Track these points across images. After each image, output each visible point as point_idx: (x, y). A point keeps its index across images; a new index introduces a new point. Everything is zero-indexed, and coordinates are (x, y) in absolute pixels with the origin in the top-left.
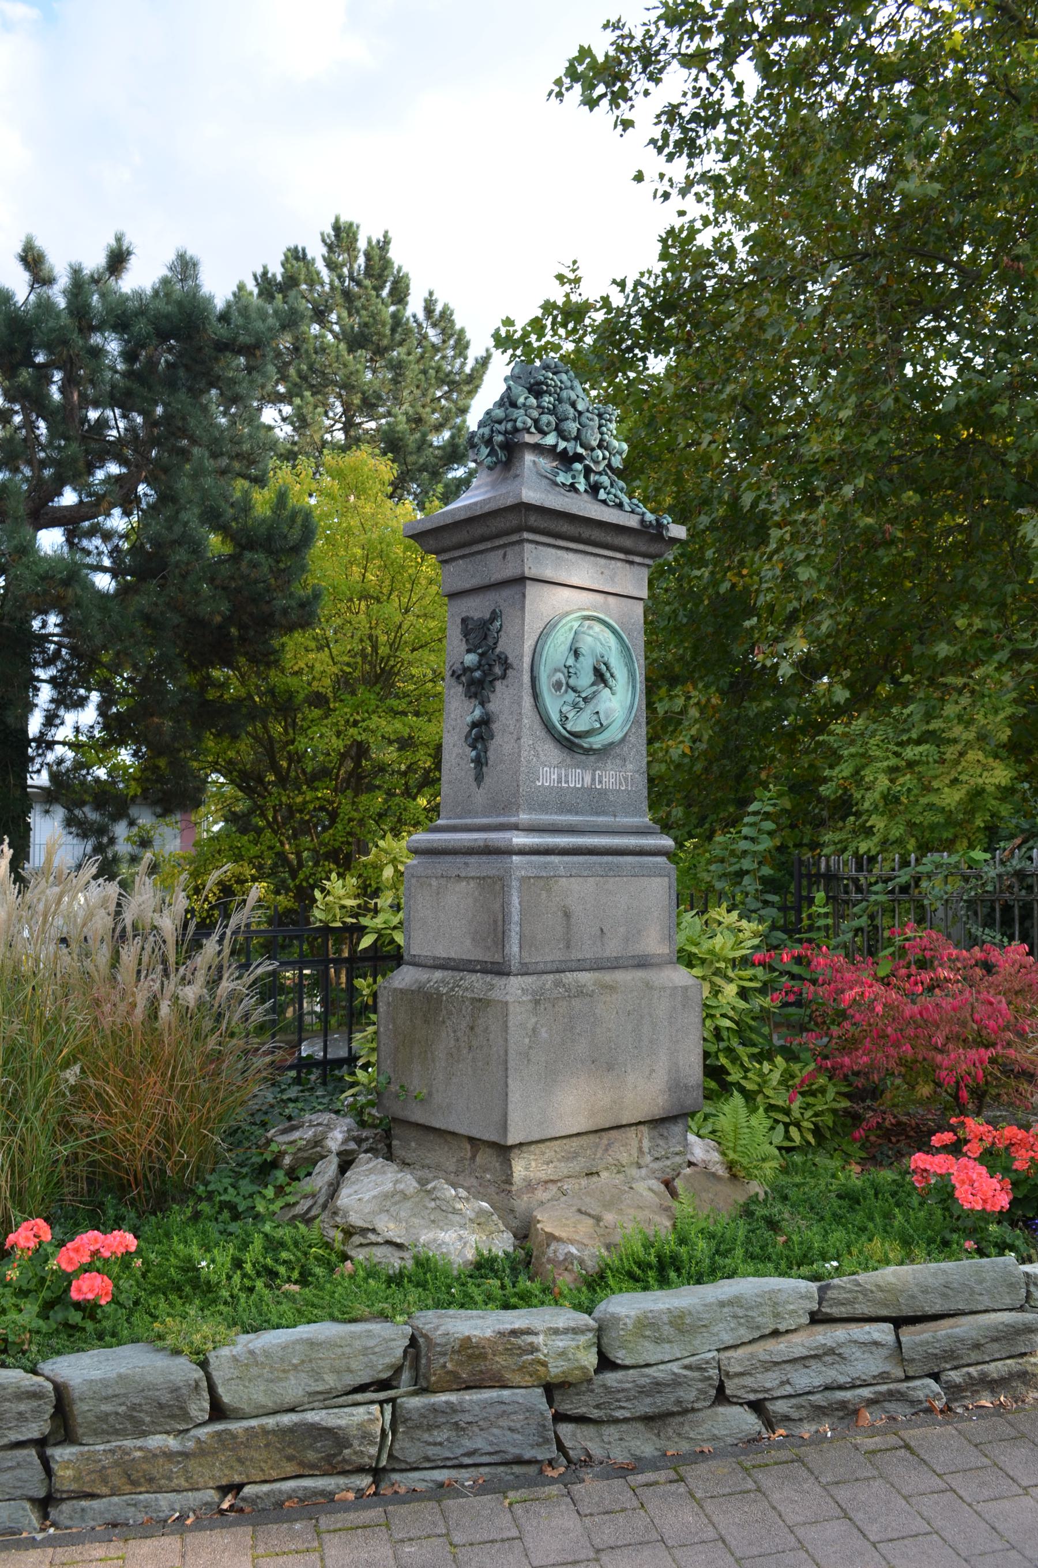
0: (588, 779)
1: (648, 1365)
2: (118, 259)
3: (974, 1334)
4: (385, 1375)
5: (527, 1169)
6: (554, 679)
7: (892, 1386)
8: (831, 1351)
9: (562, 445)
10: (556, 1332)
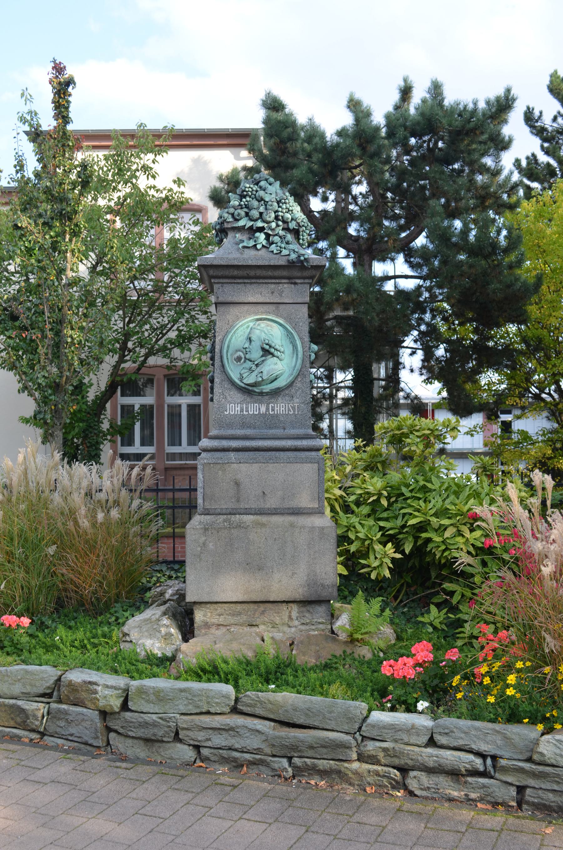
0: (263, 409)
1: (142, 712)
2: (406, 92)
3: (309, 739)
4: (48, 691)
5: (204, 616)
6: (236, 356)
7: (262, 757)
8: (232, 729)
9: (251, 223)
10: (107, 687)
